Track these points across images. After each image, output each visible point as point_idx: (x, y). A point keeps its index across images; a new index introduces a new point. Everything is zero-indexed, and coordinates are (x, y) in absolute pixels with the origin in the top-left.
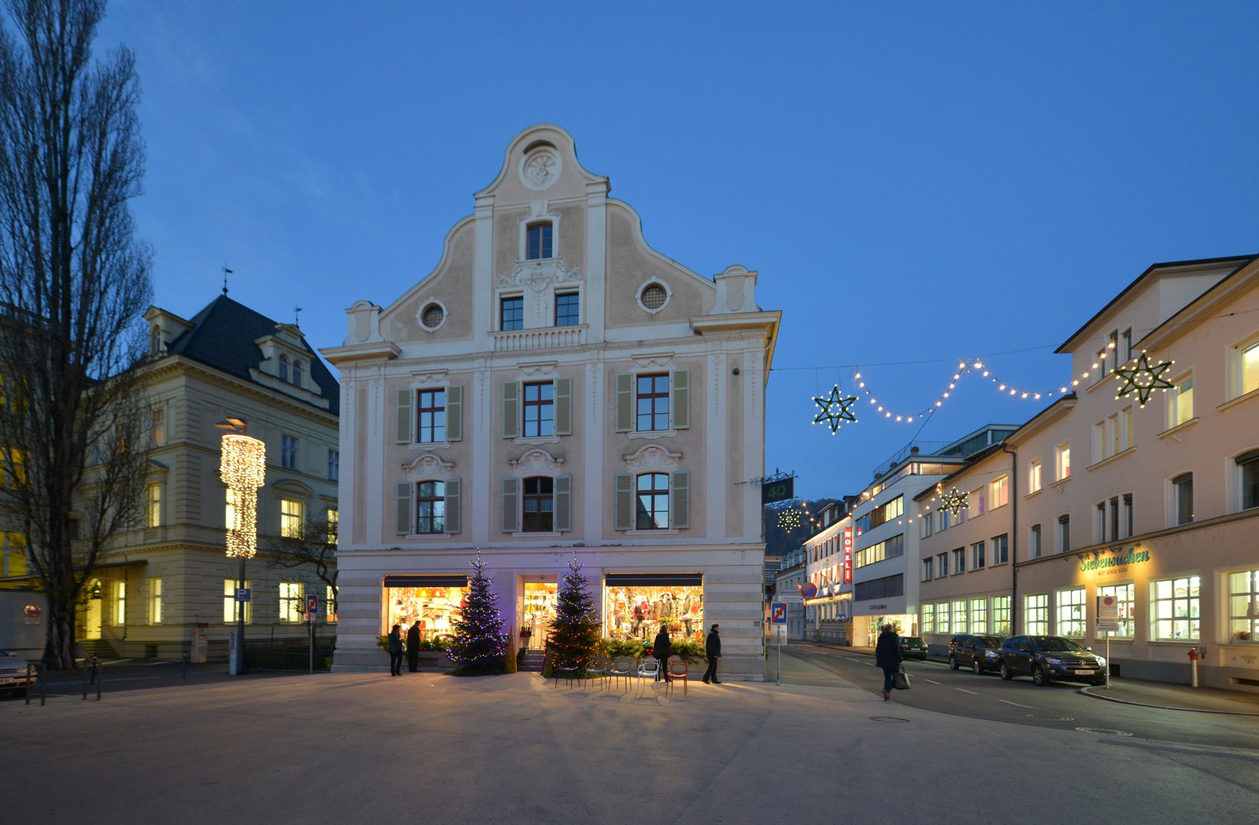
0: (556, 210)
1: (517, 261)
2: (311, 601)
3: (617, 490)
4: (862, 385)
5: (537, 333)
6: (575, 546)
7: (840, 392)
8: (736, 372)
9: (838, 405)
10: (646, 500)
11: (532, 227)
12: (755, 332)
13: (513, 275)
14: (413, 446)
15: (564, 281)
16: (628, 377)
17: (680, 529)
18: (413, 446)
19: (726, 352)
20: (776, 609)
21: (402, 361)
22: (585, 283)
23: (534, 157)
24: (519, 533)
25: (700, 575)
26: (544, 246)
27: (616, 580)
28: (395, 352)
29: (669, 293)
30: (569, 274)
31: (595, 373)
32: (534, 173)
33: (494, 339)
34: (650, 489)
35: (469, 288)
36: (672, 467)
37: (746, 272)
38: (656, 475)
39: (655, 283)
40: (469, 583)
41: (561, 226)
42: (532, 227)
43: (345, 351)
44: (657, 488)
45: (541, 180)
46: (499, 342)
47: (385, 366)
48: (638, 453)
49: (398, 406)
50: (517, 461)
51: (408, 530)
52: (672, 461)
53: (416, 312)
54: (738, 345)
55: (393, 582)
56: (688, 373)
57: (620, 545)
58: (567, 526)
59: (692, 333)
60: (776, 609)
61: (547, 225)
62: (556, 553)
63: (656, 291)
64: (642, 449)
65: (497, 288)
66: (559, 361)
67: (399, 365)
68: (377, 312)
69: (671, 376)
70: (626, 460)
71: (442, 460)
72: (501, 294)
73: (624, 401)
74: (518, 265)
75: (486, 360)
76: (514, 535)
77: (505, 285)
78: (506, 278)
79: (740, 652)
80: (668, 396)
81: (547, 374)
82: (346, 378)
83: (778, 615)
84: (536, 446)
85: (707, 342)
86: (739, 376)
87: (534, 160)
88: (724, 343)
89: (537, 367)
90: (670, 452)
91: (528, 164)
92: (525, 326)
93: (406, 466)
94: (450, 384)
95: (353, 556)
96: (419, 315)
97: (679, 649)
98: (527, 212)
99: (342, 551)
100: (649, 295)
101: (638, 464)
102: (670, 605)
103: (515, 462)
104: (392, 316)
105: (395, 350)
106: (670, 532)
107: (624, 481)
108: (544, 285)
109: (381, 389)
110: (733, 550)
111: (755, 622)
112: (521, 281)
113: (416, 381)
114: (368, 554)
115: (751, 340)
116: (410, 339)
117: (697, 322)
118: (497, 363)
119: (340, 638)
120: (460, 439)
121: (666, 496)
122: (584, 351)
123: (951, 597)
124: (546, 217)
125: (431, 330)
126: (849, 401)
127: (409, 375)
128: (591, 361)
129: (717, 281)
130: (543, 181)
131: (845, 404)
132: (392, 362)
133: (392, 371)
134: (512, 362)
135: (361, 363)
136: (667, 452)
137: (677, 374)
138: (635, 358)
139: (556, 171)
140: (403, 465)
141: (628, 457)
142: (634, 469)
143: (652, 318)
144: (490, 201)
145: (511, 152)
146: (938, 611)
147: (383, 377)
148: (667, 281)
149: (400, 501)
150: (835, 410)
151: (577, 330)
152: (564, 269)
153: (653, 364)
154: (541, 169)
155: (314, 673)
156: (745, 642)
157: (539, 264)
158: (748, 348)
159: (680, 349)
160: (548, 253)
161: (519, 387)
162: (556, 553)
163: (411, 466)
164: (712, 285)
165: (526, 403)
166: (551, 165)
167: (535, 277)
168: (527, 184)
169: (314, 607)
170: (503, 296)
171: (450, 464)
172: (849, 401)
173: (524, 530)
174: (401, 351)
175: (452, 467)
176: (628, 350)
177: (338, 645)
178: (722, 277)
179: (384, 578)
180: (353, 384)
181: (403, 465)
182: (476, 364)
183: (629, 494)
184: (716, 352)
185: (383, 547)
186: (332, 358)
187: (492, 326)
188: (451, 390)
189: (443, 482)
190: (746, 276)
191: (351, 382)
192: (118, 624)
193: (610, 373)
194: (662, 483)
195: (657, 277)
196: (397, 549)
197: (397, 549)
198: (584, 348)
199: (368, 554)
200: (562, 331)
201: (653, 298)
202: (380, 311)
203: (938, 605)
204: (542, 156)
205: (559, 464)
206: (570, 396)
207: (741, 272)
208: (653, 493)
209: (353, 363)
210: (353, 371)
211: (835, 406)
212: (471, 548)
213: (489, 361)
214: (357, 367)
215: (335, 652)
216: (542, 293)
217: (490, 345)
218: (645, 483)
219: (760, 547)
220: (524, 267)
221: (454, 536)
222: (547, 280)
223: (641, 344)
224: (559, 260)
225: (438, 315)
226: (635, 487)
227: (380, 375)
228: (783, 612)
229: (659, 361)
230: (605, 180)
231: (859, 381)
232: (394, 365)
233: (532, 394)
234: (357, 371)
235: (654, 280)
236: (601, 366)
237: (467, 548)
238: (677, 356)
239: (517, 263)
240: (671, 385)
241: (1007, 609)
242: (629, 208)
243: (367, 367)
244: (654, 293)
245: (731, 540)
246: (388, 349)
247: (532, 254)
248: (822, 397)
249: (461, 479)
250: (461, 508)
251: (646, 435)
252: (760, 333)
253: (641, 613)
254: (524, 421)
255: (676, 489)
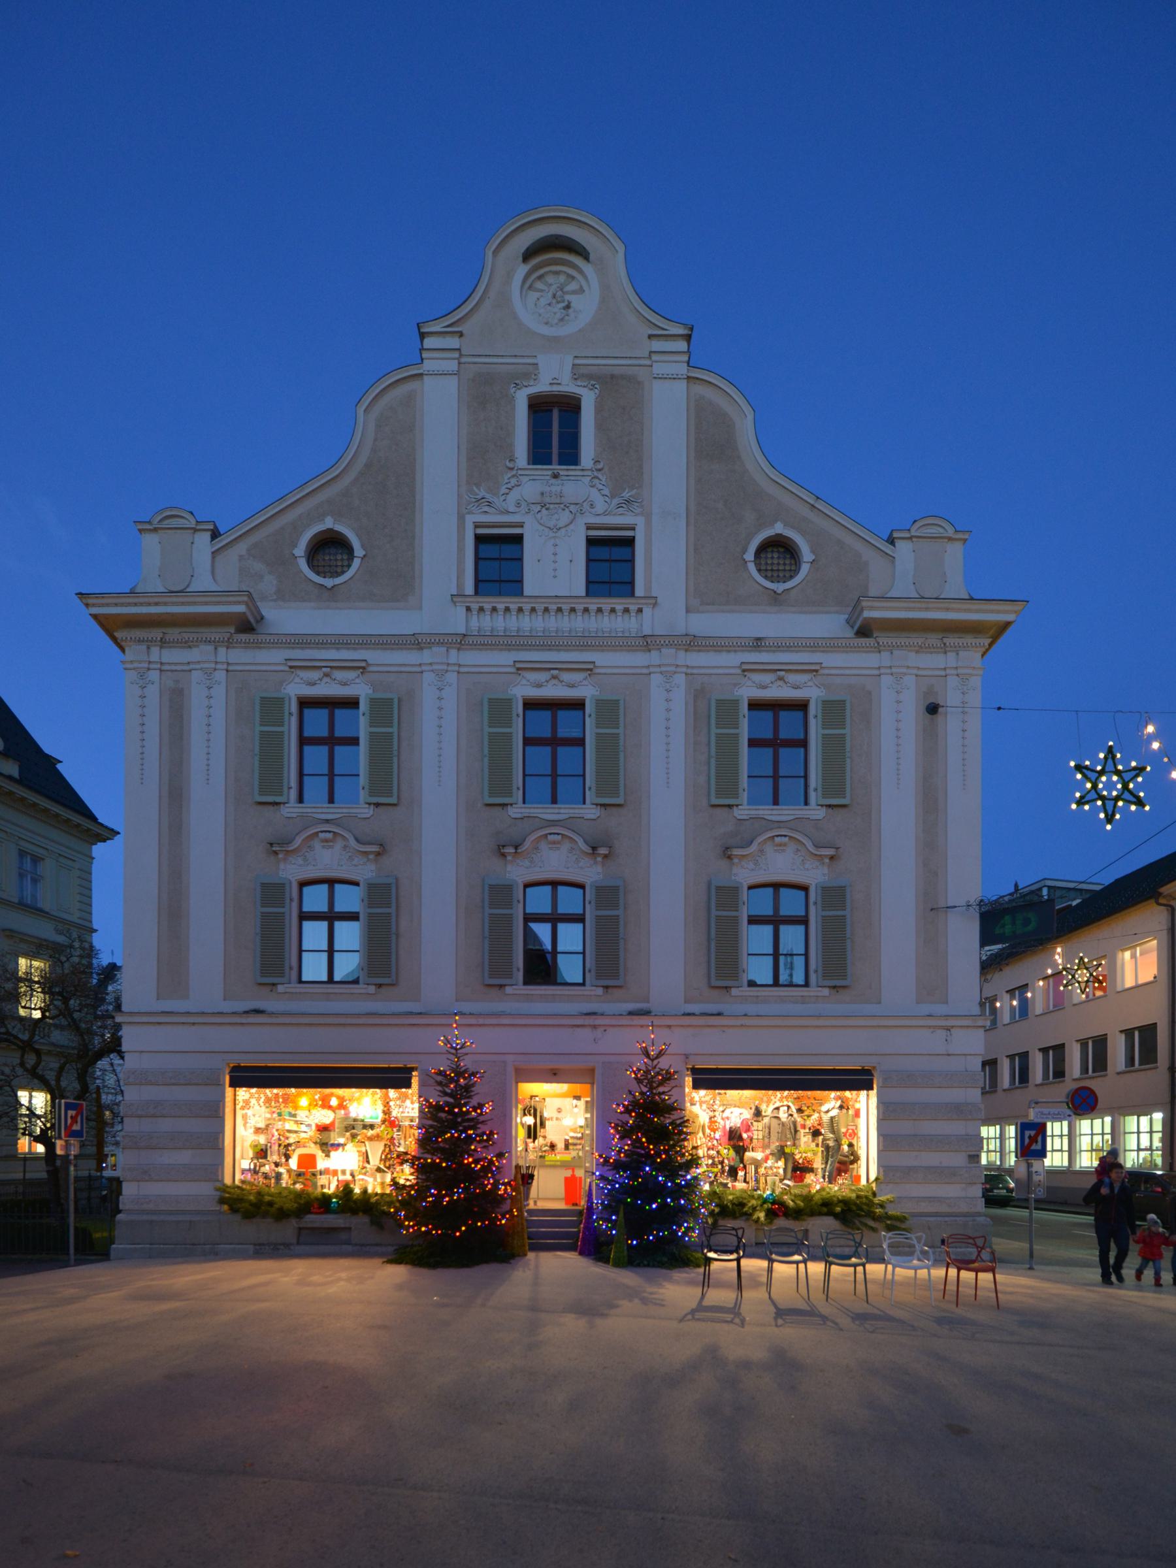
0: (590, 377)
1: (510, 465)
2: (71, 1113)
3: (620, 912)
4: (1156, 745)
5: (554, 607)
6: (631, 1013)
7: (1119, 756)
8: (933, 709)
9: (1115, 778)
10: (543, 931)
11: (540, 407)
12: (969, 640)
13: (503, 490)
14: (292, 809)
15: (605, 514)
16: (508, 702)
17: (834, 987)
18: (292, 809)
19: (456, 668)
20: (1027, 1133)
21: (263, 637)
22: (648, 523)
23: (541, 271)
24: (517, 987)
25: (868, 1072)
26: (560, 447)
27: (711, 1079)
28: (252, 620)
29: (359, 551)
30: (616, 501)
31: (668, 691)
32: (543, 302)
33: (464, 609)
34: (771, 913)
35: (408, 506)
36: (365, 871)
37: (950, 532)
38: (337, 887)
39: (780, 535)
40: (415, 1082)
41: (599, 409)
42: (540, 407)
43: (141, 604)
44: (339, 907)
45: (558, 316)
46: (475, 618)
47: (229, 644)
48: (754, 847)
49: (258, 728)
50: (516, 848)
51: (281, 974)
52: (365, 860)
53: (294, 545)
54: (934, 661)
55: (246, 1077)
56: (622, 702)
57: (719, 1014)
58: (616, 976)
59: (850, 633)
60: (1027, 1133)
61: (570, 407)
62: (595, 1027)
63: (778, 552)
64: (761, 839)
65: (470, 513)
66: (370, 662)
67: (258, 645)
68: (208, 535)
69: (363, 706)
70: (730, 857)
71: (357, 840)
72: (477, 526)
73: (270, 747)
74: (514, 472)
75: (148, 648)
76: (508, 990)
77: (486, 509)
78: (487, 496)
79: (944, 1209)
80: (749, 740)
81: (345, 684)
82: (140, 662)
83: (1030, 1144)
84: (553, 823)
85: (422, 649)
86: (939, 718)
87: (540, 278)
88: (682, 654)
89: (555, 672)
90: (817, 846)
91: (527, 285)
92: (527, 590)
93: (278, 847)
94: (370, 691)
95: (159, 1023)
96: (300, 550)
97: (836, 1205)
98: (531, 373)
99: (131, 1014)
100: (766, 558)
101: (751, 866)
102: (795, 1123)
103: (512, 850)
104: (242, 548)
105: (252, 614)
106: (588, 990)
107: (272, 893)
108: (565, 517)
109: (219, 692)
110: (930, 1027)
111: (970, 1156)
112: (518, 505)
113: (297, 680)
114: (191, 1020)
115: (663, 650)
116: (281, 596)
117: (872, 608)
118: (471, 658)
119: (128, 1189)
120: (393, 800)
121: (579, 927)
122: (647, 648)
123: (1003, 1118)
124: (568, 387)
125: (329, 582)
126: (1134, 773)
127: (283, 668)
128: (663, 669)
129: (898, 543)
130: (562, 320)
131: (1127, 776)
132: (244, 637)
133: (240, 657)
134: (505, 659)
135: (173, 633)
136: (352, 842)
137: (600, 703)
138: (746, 670)
139: (586, 305)
140: (271, 844)
141: (736, 852)
142: (292, 871)
143: (776, 599)
144: (453, 342)
145: (496, 252)
146: (1007, 1136)
147: (225, 666)
148: (803, 533)
149: (264, 915)
150: (1110, 786)
151: (633, 608)
152: (606, 491)
153: (780, 683)
154: (554, 296)
155: (78, 1263)
156: (950, 1191)
157: (556, 476)
158: (431, 664)
159: (832, 660)
160: (571, 456)
161: (517, 708)
162: (595, 1027)
163: (290, 849)
164: (888, 548)
165: (303, 741)
166: (574, 292)
167: (548, 500)
168: (528, 319)
169: (76, 1127)
170: (481, 531)
171: (375, 848)
172: (1134, 773)
173: (526, 983)
174: (262, 618)
175: (378, 854)
176: (732, 655)
177: (125, 1202)
178: (908, 535)
179: (227, 1071)
180: (154, 675)
181: (271, 844)
182: (426, 656)
183: (509, 919)
184: (206, 665)
185: (227, 1007)
186: (107, 616)
187: (460, 585)
188: (373, 702)
189: (357, 884)
190: (950, 539)
191: (151, 672)
192: (1010, 1166)
193: (698, 694)
194: (347, 899)
195: (786, 525)
196: (258, 1012)
197: (258, 1012)
198: (648, 643)
199: (191, 1020)
200: (604, 607)
201: (772, 564)
202: (215, 534)
203: (1007, 1127)
204: (557, 273)
205: (599, 859)
206: (395, 730)
207: (941, 530)
208: (554, 919)
209: (156, 633)
210: (155, 650)
211: (1109, 779)
212: (420, 1014)
213: (155, 650)
214: (163, 643)
215: (120, 1217)
216: (563, 530)
217: (456, 621)
218: (540, 900)
219: (980, 1023)
220: (525, 479)
221: (383, 990)
222: (572, 508)
223: (758, 643)
224: (596, 474)
225: (339, 557)
226: (295, 905)
227: (216, 663)
228: (1027, 1141)
229: (566, 677)
230: (686, 332)
231: (1152, 738)
232: (247, 646)
233: (317, 724)
234: (164, 651)
235: (779, 528)
236: (680, 679)
237: (411, 1013)
238: (826, 672)
239: (512, 469)
240: (363, 722)
241: (1061, 1136)
242: (730, 390)
243: (187, 645)
244: (776, 555)
245: (926, 1009)
246: (241, 608)
247: (539, 455)
248: (1087, 763)
249: (397, 879)
250: (397, 935)
251: (766, 812)
252: (978, 641)
253: (740, 1138)
254: (301, 775)
255: (824, 913)
